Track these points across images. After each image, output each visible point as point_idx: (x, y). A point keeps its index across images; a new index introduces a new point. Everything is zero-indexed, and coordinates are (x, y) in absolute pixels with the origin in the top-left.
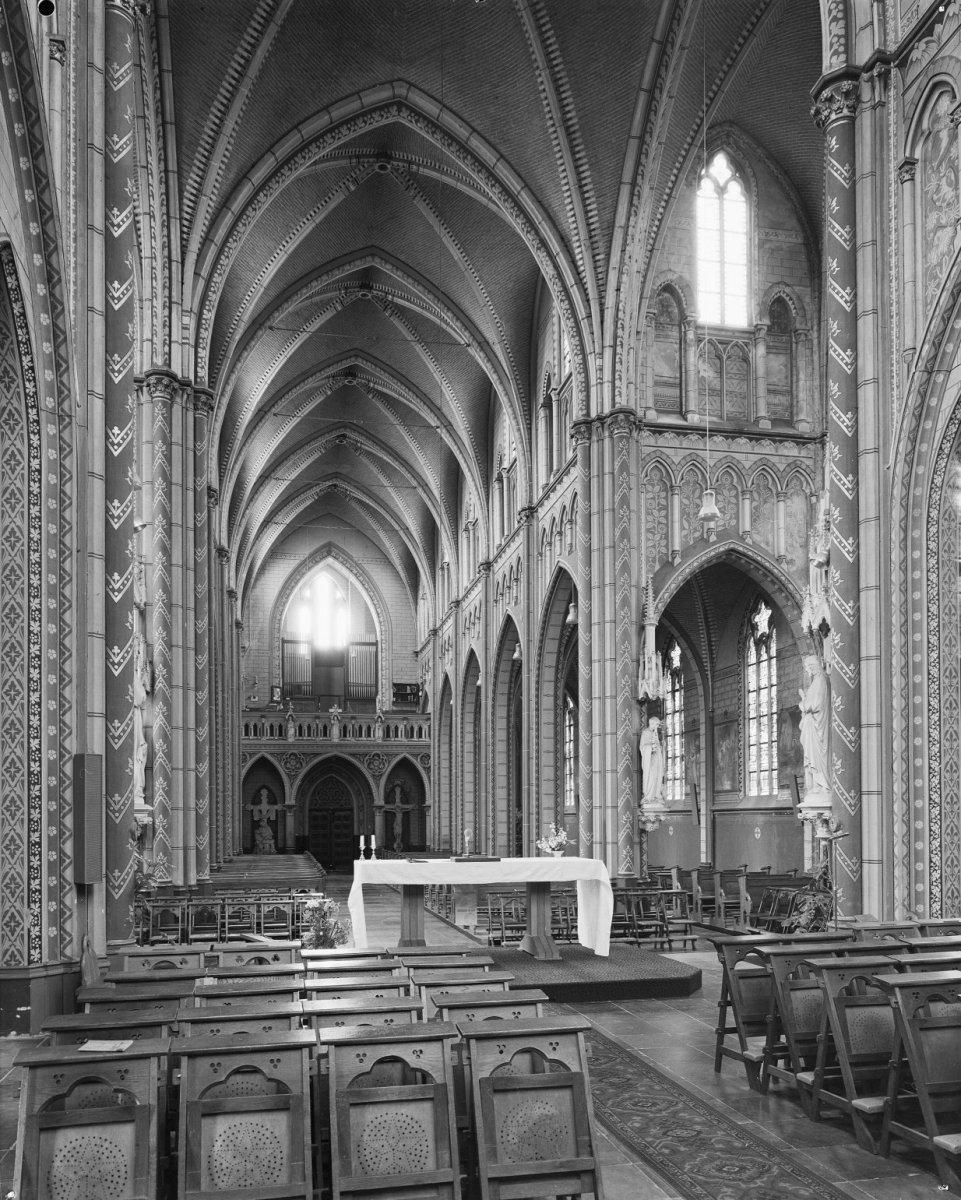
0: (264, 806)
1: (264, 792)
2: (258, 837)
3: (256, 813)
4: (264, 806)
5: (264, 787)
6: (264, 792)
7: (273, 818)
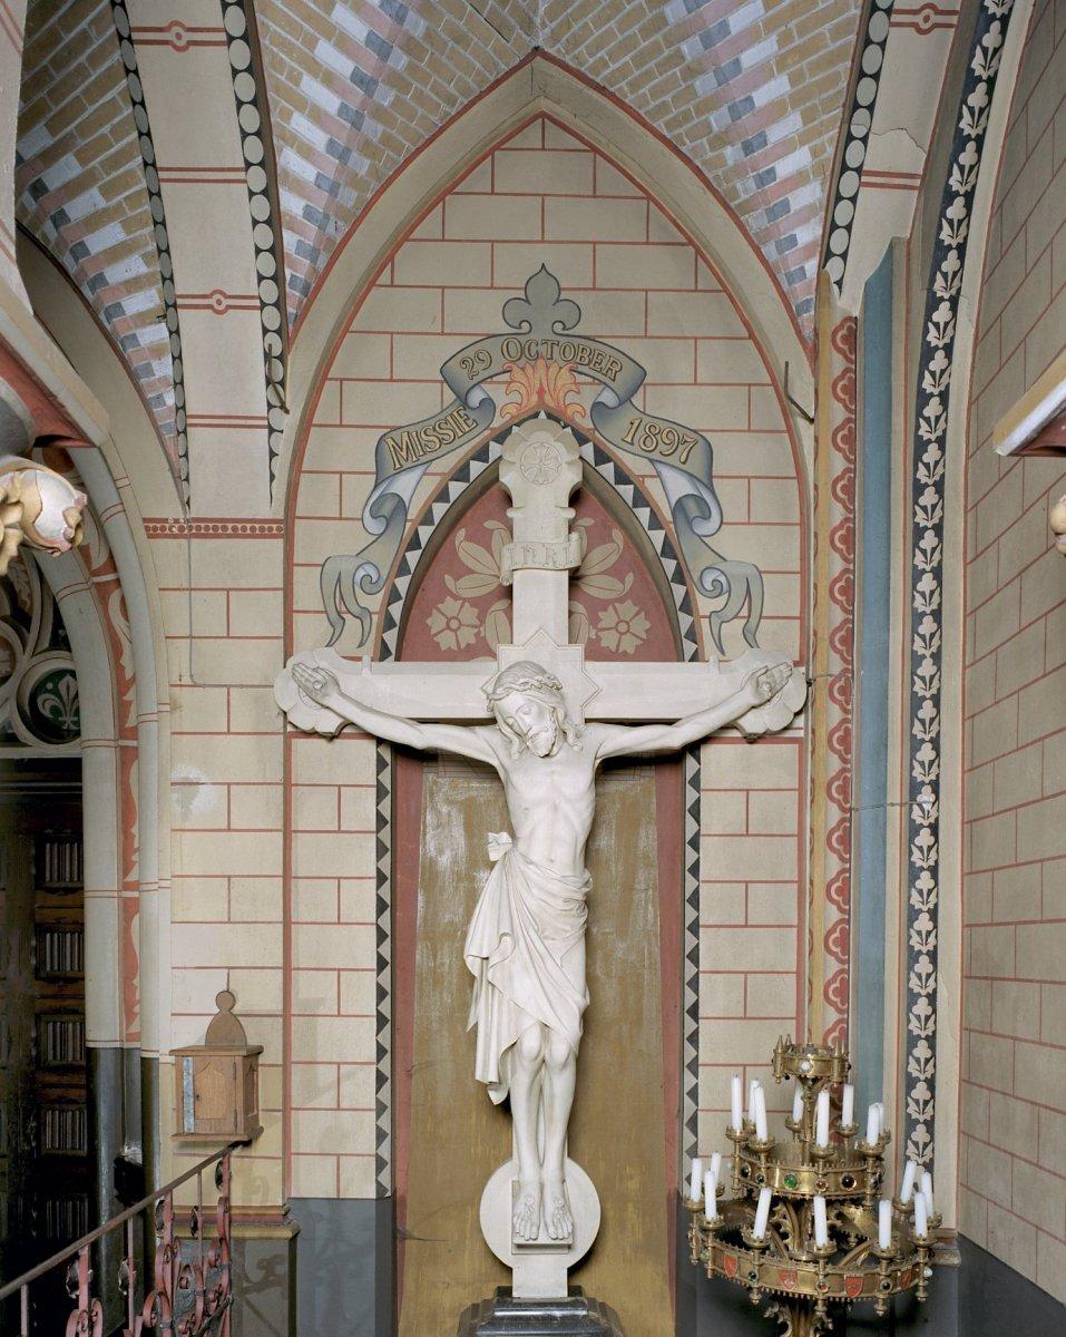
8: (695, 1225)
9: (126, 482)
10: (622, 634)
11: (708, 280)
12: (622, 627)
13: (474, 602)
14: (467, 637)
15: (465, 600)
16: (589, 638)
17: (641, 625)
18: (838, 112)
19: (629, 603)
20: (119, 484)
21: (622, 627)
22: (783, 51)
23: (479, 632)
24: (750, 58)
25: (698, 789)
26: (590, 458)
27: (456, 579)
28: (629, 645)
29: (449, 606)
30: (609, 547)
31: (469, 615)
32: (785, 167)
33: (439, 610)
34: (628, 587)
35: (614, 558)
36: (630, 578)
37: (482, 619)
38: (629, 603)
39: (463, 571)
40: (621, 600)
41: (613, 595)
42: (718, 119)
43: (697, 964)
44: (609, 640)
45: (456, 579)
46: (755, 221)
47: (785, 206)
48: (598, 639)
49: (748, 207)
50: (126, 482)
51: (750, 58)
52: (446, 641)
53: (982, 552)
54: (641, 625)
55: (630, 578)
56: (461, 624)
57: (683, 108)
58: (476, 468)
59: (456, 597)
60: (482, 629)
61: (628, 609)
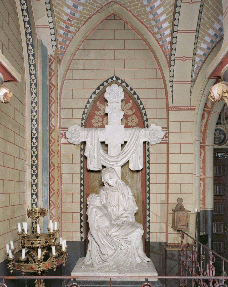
0: (114, 131)
1: (115, 95)
2: (96, 219)
3: (93, 151)
4: (114, 131)
5: (116, 80)
6: (115, 95)
7: (137, 164)
8: (157, 252)
9: (202, 90)
10: (133, 122)
11: (138, 36)
12: (133, 121)
13: (101, 116)
14: (100, 124)
15: (99, 116)
16: (126, 123)
17: (137, 120)
18: (173, 8)
19: (134, 115)
20: (203, 90)
21: (133, 121)
22: (165, 9)
23: (103, 123)
24: (159, 12)
25: (149, 164)
26: (125, 85)
27: (97, 112)
28: (134, 124)
29: (96, 117)
30: (130, 104)
31: (100, 119)
32: (162, 19)
33: (94, 118)
34: (134, 112)
35: (130, 106)
36: (134, 110)
37: (103, 120)
38: (134, 115)
39: (99, 110)
40: (132, 115)
41: (131, 114)
42: (154, 23)
43: (149, 211)
44: (130, 123)
45: (97, 112)
46: (158, 36)
47: (162, 27)
48: (128, 123)
49: (155, 33)
50: (202, 90)
51: (159, 12)
52: (96, 125)
53: (102, 21)
54: (137, 120)
55: (134, 110)
56: (96, 122)
57: (150, 26)
58: (101, 87)
59: (97, 116)
60: (103, 122)
61: (134, 117)
